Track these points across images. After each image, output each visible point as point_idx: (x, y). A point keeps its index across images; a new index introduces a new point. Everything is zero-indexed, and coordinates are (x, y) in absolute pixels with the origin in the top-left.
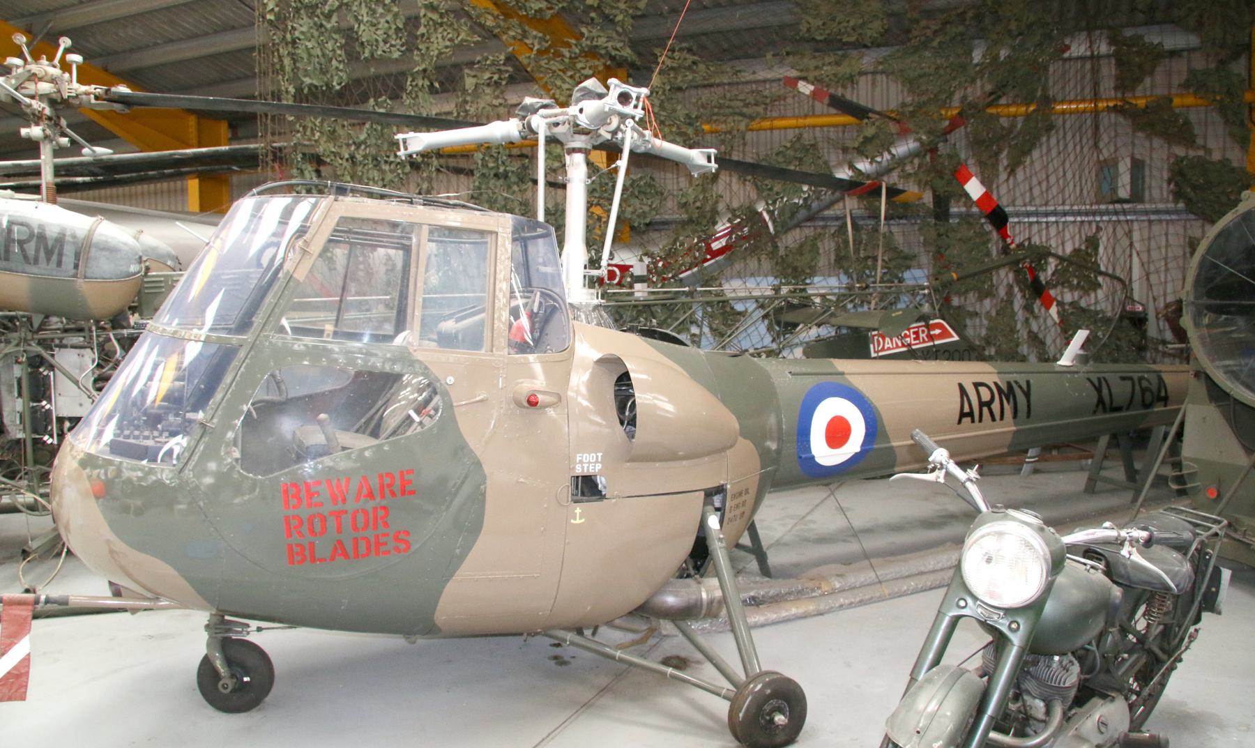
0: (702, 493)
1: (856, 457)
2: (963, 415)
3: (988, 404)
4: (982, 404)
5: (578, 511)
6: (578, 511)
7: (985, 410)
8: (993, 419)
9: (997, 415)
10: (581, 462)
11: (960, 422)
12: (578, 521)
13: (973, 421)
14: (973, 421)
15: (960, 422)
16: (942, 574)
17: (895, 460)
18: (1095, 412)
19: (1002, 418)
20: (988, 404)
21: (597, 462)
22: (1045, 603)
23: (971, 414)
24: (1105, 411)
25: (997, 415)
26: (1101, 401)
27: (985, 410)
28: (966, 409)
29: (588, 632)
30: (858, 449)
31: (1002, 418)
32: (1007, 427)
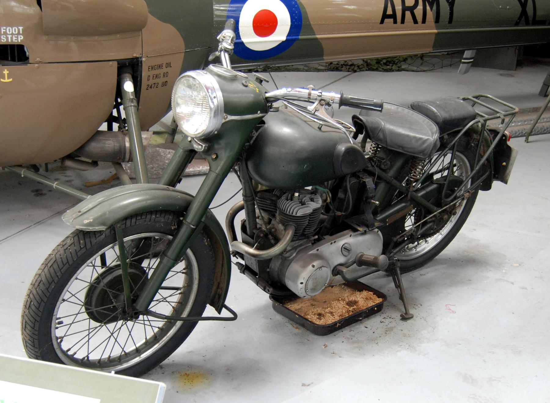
0: (115, 64)
1: (282, 47)
2: (385, 16)
3: (412, 9)
4: (405, 9)
5: (6, 72)
6: (6, 72)
7: (408, 13)
8: (416, 22)
9: (419, 17)
10: (5, 33)
11: (382, 22)
12: (6, 80)
13: (395, 22)
14: (395, 22)
15: (382, 22)
16: (178, 193)
17: (323, 51)
18: (517, 24)
19: (424, 21)
20: (412, 9)
21: (19, 34)
22: (442, 264)
23: (393, 16)
24: (527, 24)
25: (419, 17)
26: (524, 12)
27: (408, 13)
28: (389, 12)
29: (42, 171)
30: (284, 38)
31: (424, 21)
32: (430, 29)
